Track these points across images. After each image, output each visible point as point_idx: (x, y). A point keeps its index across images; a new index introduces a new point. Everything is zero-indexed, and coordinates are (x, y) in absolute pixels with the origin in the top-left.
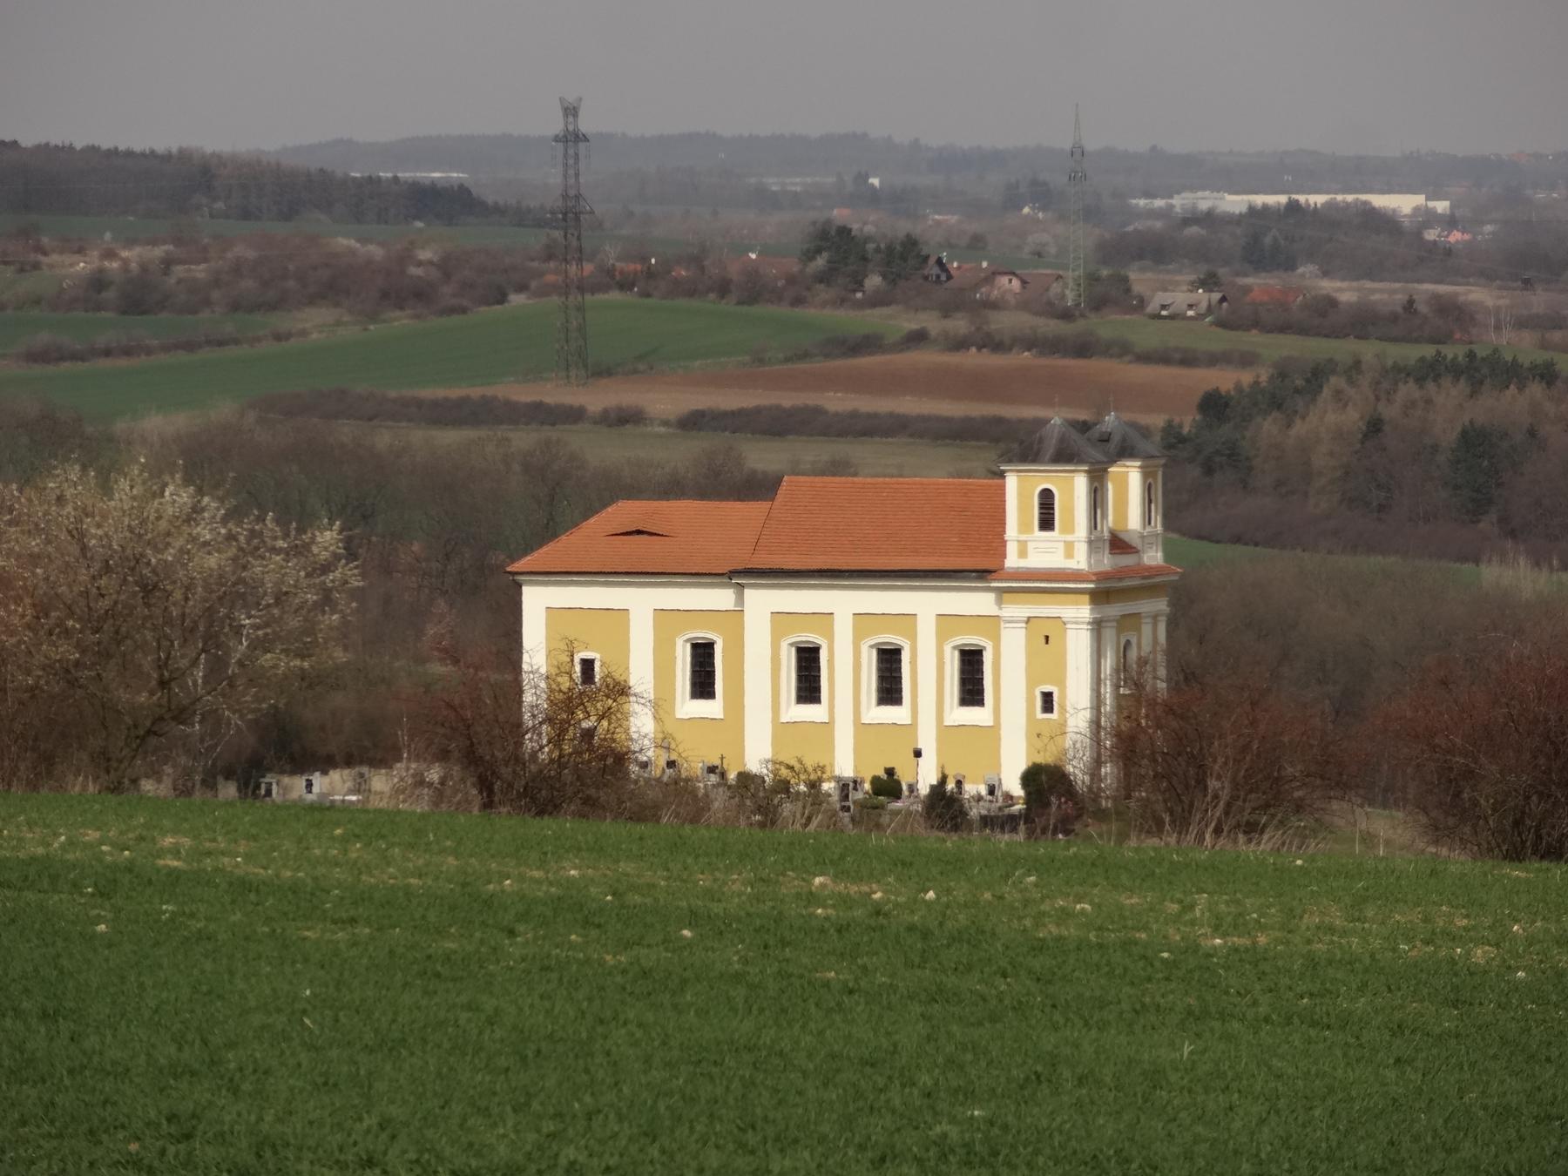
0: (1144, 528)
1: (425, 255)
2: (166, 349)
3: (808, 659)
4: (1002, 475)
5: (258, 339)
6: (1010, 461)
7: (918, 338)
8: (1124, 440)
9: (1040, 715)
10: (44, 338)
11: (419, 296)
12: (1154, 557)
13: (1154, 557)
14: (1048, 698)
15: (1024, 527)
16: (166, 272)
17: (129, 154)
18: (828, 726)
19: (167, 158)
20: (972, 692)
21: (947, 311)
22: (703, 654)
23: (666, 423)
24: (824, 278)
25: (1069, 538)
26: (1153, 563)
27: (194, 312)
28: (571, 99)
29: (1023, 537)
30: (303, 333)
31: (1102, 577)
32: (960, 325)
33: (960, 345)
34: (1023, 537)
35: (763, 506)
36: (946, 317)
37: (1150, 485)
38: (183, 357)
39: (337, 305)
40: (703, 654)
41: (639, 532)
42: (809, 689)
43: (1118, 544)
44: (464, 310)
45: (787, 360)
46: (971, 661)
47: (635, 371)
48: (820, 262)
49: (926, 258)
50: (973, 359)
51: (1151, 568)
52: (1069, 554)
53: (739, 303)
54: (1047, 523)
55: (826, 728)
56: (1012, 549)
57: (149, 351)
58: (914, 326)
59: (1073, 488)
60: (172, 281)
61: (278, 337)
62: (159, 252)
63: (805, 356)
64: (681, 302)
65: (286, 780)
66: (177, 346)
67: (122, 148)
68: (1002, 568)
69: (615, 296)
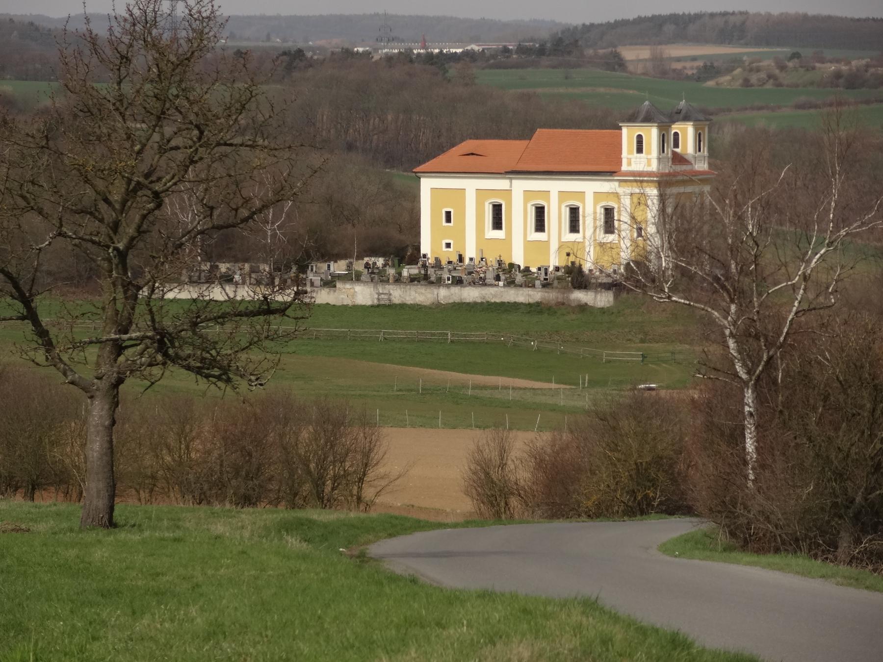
0: (696, 153)
3: (540, 212)
4: (620, 128)
6: (623, 121)
8: (687, 113)
10: (803, 99)
12: (702, 166)
13: (702, 166)
15: (630, 152)
16: (866, 71)
22: (497, 209)
25: (649, 157)
26: (701, 169)
29: (630, 156)
31: (662, 175)
34: (630, 156)
35: (525, 143)
40: (497, 209)
41: (473, 154)
42: (540, 226)
43: (678, 159)
54: (640, 150)
56: (624, 162)
59: (652, 134)
60: (869, 74)
62: (864, 62)
65: (319, 265)
68: (620, 170)
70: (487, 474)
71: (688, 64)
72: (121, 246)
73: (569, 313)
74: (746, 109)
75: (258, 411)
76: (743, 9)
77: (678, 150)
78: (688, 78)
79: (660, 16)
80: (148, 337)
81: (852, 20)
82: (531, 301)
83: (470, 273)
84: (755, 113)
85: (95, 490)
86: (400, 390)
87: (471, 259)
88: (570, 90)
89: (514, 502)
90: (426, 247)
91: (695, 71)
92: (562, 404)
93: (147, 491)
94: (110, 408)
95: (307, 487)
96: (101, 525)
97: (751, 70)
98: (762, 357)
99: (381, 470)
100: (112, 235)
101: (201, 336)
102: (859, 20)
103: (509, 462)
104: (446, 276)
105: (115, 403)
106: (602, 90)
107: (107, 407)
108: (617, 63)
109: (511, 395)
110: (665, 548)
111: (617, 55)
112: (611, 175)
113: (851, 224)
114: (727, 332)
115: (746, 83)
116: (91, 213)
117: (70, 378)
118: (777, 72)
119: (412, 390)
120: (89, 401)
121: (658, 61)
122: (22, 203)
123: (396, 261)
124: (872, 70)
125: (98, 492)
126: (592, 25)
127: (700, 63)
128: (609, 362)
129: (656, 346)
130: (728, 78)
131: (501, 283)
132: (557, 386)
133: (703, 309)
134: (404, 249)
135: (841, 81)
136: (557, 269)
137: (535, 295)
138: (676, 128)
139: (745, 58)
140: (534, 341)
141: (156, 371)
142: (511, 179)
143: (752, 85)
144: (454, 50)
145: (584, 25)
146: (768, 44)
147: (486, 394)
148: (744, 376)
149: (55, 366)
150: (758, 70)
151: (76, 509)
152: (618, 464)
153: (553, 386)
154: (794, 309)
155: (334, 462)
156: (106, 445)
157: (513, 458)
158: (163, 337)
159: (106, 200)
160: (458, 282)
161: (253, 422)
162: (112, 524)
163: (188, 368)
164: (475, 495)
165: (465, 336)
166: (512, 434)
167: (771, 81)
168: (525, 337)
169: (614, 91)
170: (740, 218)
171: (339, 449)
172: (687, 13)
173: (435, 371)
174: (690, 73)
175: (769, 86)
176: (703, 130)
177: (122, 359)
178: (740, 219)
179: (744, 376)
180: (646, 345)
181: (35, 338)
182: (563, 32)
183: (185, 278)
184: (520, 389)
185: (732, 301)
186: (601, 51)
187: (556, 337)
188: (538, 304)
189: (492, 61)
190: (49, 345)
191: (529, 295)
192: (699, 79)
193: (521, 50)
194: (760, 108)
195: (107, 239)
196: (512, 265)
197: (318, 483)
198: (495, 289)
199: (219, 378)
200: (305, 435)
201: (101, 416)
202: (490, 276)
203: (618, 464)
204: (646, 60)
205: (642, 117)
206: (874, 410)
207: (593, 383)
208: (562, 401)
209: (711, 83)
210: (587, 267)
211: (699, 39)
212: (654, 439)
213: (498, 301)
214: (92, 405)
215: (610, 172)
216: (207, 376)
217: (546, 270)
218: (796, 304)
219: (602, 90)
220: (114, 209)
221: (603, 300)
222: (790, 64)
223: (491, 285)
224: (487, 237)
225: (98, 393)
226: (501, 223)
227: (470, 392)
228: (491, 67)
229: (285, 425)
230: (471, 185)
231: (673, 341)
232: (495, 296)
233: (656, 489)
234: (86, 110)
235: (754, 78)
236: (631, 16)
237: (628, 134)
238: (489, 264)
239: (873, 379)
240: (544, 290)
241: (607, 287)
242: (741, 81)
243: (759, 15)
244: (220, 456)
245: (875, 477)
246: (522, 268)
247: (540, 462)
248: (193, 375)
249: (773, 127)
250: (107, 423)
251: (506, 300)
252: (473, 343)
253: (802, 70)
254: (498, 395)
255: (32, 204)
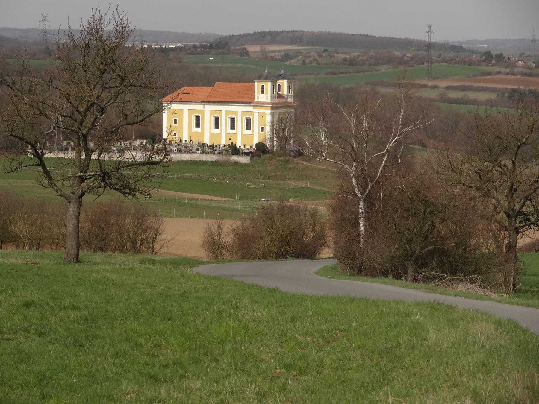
1: (408, 55)
2: (354, 72)
3: (217, 120)
5: (372, 71)
7: (499, 73)
9: (261, 132)
10: (329, 70)
11: (406, 63)
12: (291, 100)
13: (291, 100)
14: (262, 128)
15: (258, 93)
17: (396, 38)
18: (252, 135)
19: (404, 39)
20: (248, 127)
21: (506, 68)
22: (198, 118)
23: (443, 88)
24: (484, 61)
25: (267, 95)
27: (362, 66)
28: (430, 25)
29: (258, 95)
30: (381, 70)
31: (273, 104)
32: (508, 70)
33: (507, 74)
34: (258, 95)
35: (210, 88)
36: (506, 69)
37: (290, 85)
38: (357, 74)
39: (389, 65)
40: (198, 118)
41: (187, 93)
42: (217, 126)
43: (280, 96)
44: (413, 66)
45: (473, 76)
46: (248, 121)
47: (442, 78)
48: (484, 58)
49: (504, 57)
50: (509, 77)
51: (289, 102)
52: (267, 99)
53: (468, 66)
54: (263, 92)
55: (236, 135)
56: (256, 97)
57: (350, 73)
58: (499, 70)
59: (268, 85)
60: (359, 60)
61: (376, 71)
62: (357, 54)
63: (476, 76)
64: (457, 65)
66: (356, 72)
67: (395, 37)
69: (444, 64)
70: (212, 239)
71: (277, 54)
72: (84, 132)
73: (230, 166)
74: (304, 74)
75: (106, 209)
76: (301, 29)
77: (280, 93)
78: (277, 60)
79: (264, 32)
80: (97, 175)
81: (350, 35)
82: (213, 160)
83: (185, 147)
84: (307, 76)
85: (70, 245)
86: (155, 200)
87: (186, 141)
88: (224, 65)
89: (224, 252)
90: (165, 136)
91: (280, 57)
92: (228, 207)
93: (55, 245)
94: (78, 208)
95: (129, 244)
96: (73, 262)
97: (306, 57)
98: (368, 187)
99: (163, 236)
100: (80, 127)
101: (121, 174)
102: (353, 35)
103: (222, 233)
104: (174, 148)
105: (80, 205)
106: (238, 65)
107: (76, 207)
108: (245, 53)
109: (205, 203)
110: (317, 273)
111: (245, 49)
112: (250, 104)
113: (409, 126)
114: (352, 175)
115: (304, 63)
116: (70, 117)
117: (59, 193)
118: (318, 58)
119: (160, 200)
120: (68, 204)
121: (263, 52)
122: (37, 112)
123: (152, 142)
124: (360, 58)
125: (72, 246)
126: (233, 35)
127: (283, 54)
128: (249, 188)
129: (271, 181)
130: (296, 60)
131: (199, 152)
132: (226, 199)
133: (341, 164)
134: (155, 136)
135: (347, 62)
136: (225, 146)
137: (214, 158)
138: (279, 82)
139: (303, 51)
140: (214, 178)
141: (101, 190)
142: (204, 105)
143: (306, 64)
144: (171, 46)
145: (230, 35)
146: (313, 45)
147: (194, 202)
148: (360, 196)
149: (52, 187)
150: (309, 57)
151: (61, 253)
152: (273, 235)
153: (224, 199)
154: (383, 165)
155: (141, 233)
156: (76, 225)
157: (224, 232)
158: (104, 175)
159: (78, 111)
160: (180, 151)
161: (104, 214)
162: (78, 261)
163: (116, 189)
164: (206, 249)
165: (183, 176)
166: (224, 221)
167: (315, 62)
168: (210, 177)
169: (245, 66)
170: (359, 122)
171: (144, 227)
172: (276, 30)
173: (170, 191)
174: (278, 58)
175: (314, 64)
176: (291, 83)
177: (84, 184)
178: (360, 123)
179: (360, 196)
180: (265, 181)
181: (44, 174)
182: (220, 39)
183: (55, 147)
184: (209, 200)
185: (354, 161)
186: (238, 47)
187: (224, 177)
188: (216, 162)
189: (189, 51)
190: (49, 178)
191: (212, 158)
192: (282, 61)
193: (202, 46)
194: (310, 74)
195: (78, 129)
196: (204, 144)
197: (134, 242)
198: (197, 154)
199: (129, 194)
200: (128, 220)
201: (74, 211)
202: (194, 149)
203: (273, 235)
204: (258, 52)
205: (264, 77)
206: (425, 212)
207: (242, 198)
208: (228, 206)
209: (288, 63)
210: (239, 144)
211: (281, 43)
212: (289, 223)
213: (198, 160)
214: (69, 206)
215: (249, 101)
216: (124, 193)
217: (220, 146)
218: (383, 162)
219: (238, 65)
220: (81, 115)
221: (244, 160)
222: (324, 54)
223: (195, 153)
224: (193, 131)
225: (72, 200)
226: (199, 125)
227: (186, 201)
228: (188, 54)
229: (119, 215)
230: (186, 108)
231: (277, 179)
232: (196, 158)
233: (290, 246)
234: (68, 69)
235: (307, 61)
236: (251, 31)
237: (257, 85)
238: (194, 143)
239: (425, 197)
240: (219, 155)
241: (247, 154)
242: (301, 62)
243: (309, 32)
244: (89, 229)
245: (425, 242)
246: (209, 145)
247: (236, 232)
248: (117, 192)
249: (317, 83)
250: (76, 214)
251: (201, 160)
252: (187, 179)
253: (329, 57)
254: (199, 203)
255: (42, 113)
